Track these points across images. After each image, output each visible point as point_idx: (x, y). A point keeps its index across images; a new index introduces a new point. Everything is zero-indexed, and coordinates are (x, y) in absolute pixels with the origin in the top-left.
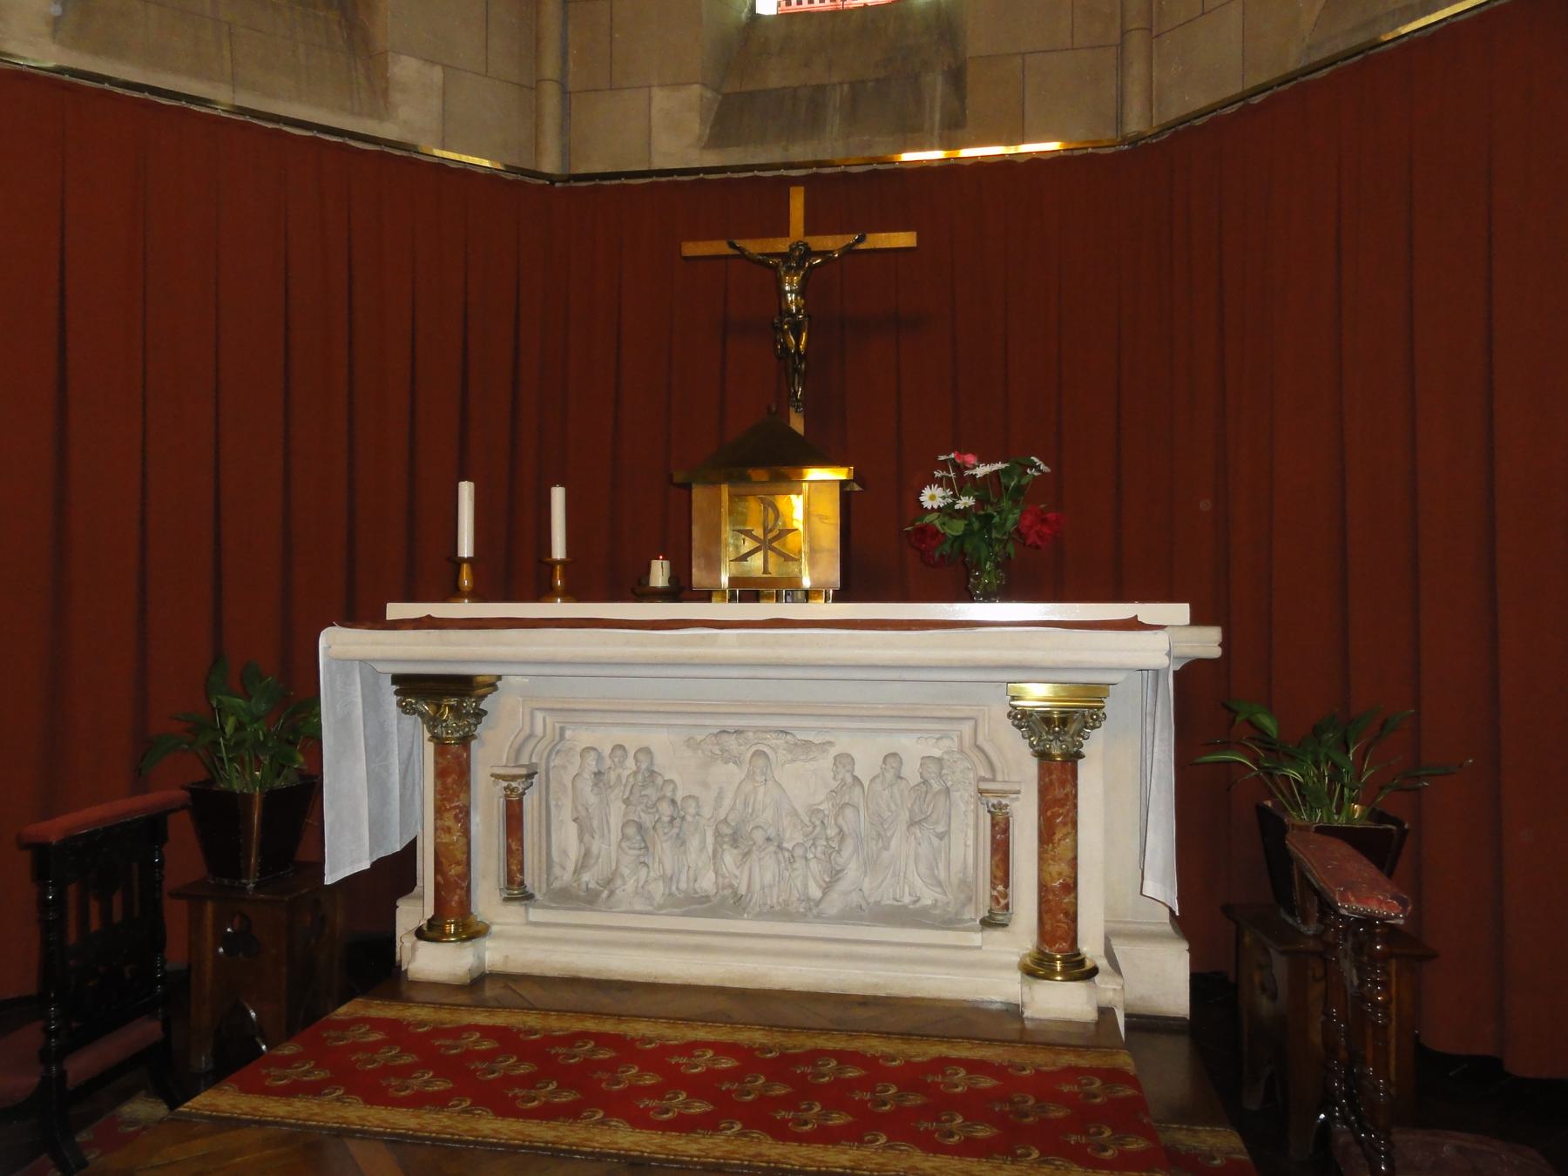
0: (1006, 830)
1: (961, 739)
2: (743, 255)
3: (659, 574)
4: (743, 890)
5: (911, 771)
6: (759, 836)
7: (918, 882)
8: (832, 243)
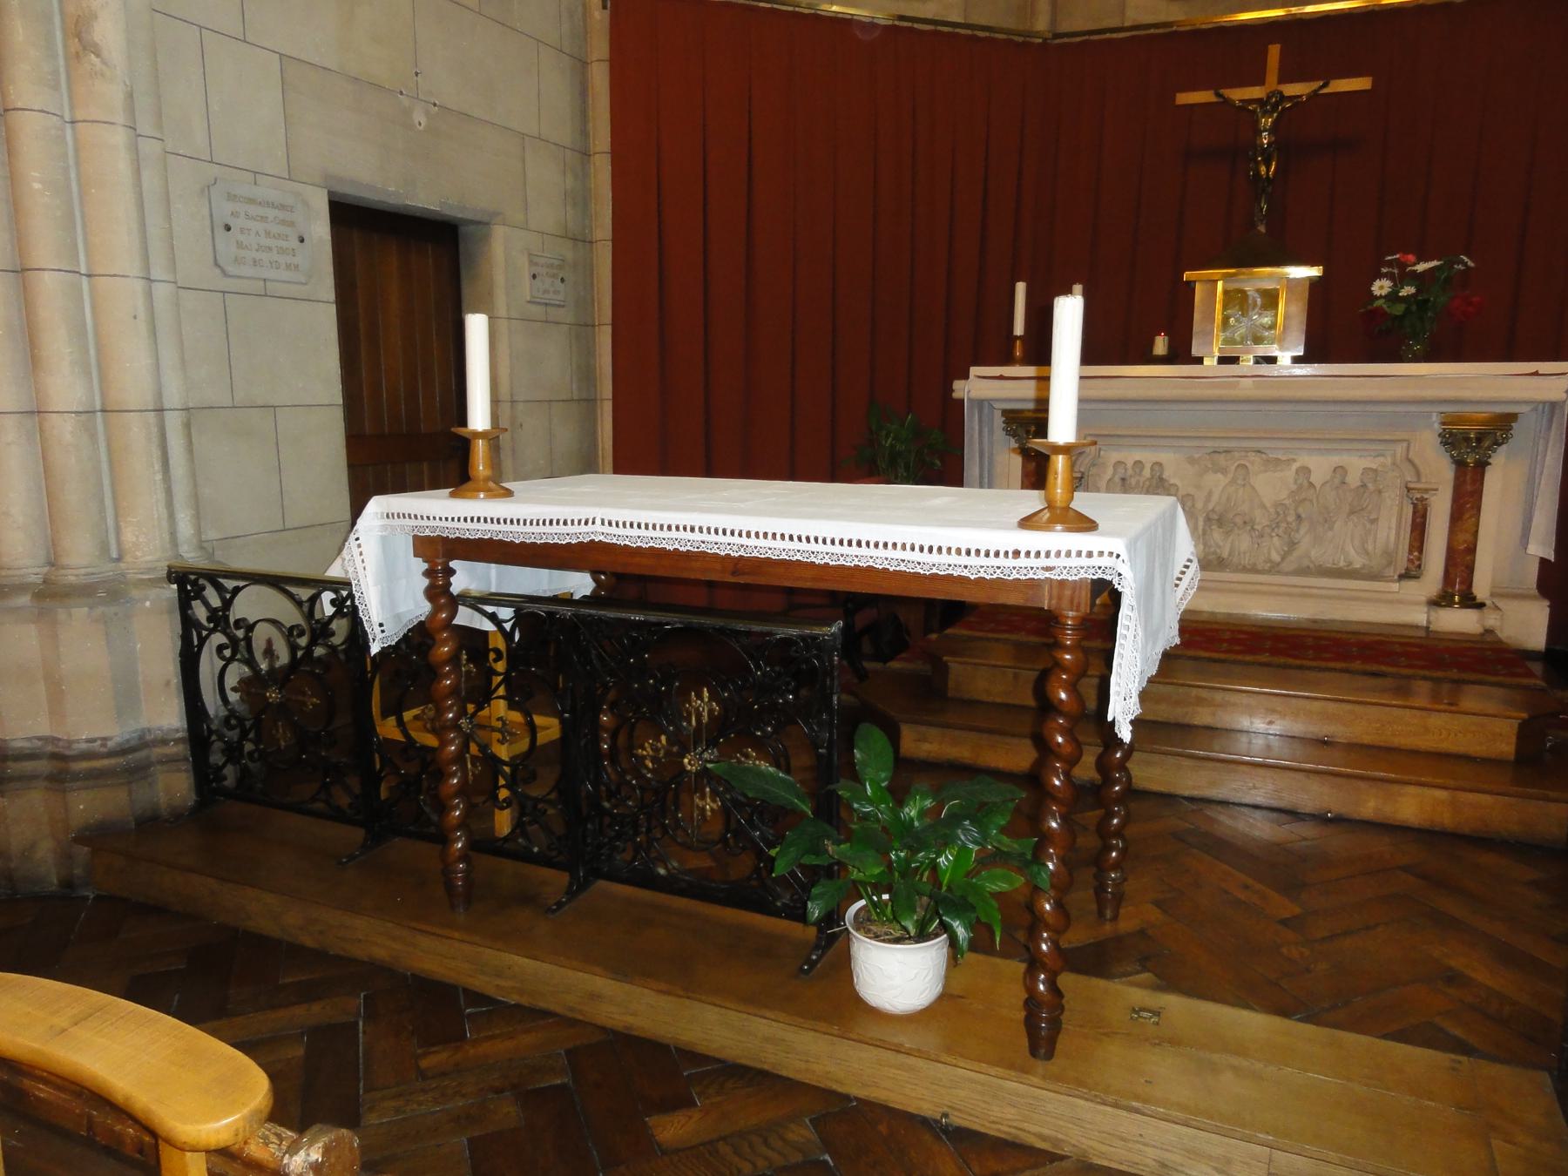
0: (1424, 516)
1: (1394, 456)
2: (1227, 102)
3: (1160, 346)
4: (1225, 555)
5: (1354, 479)
6: (1239, 520)
7: (1352, 552)
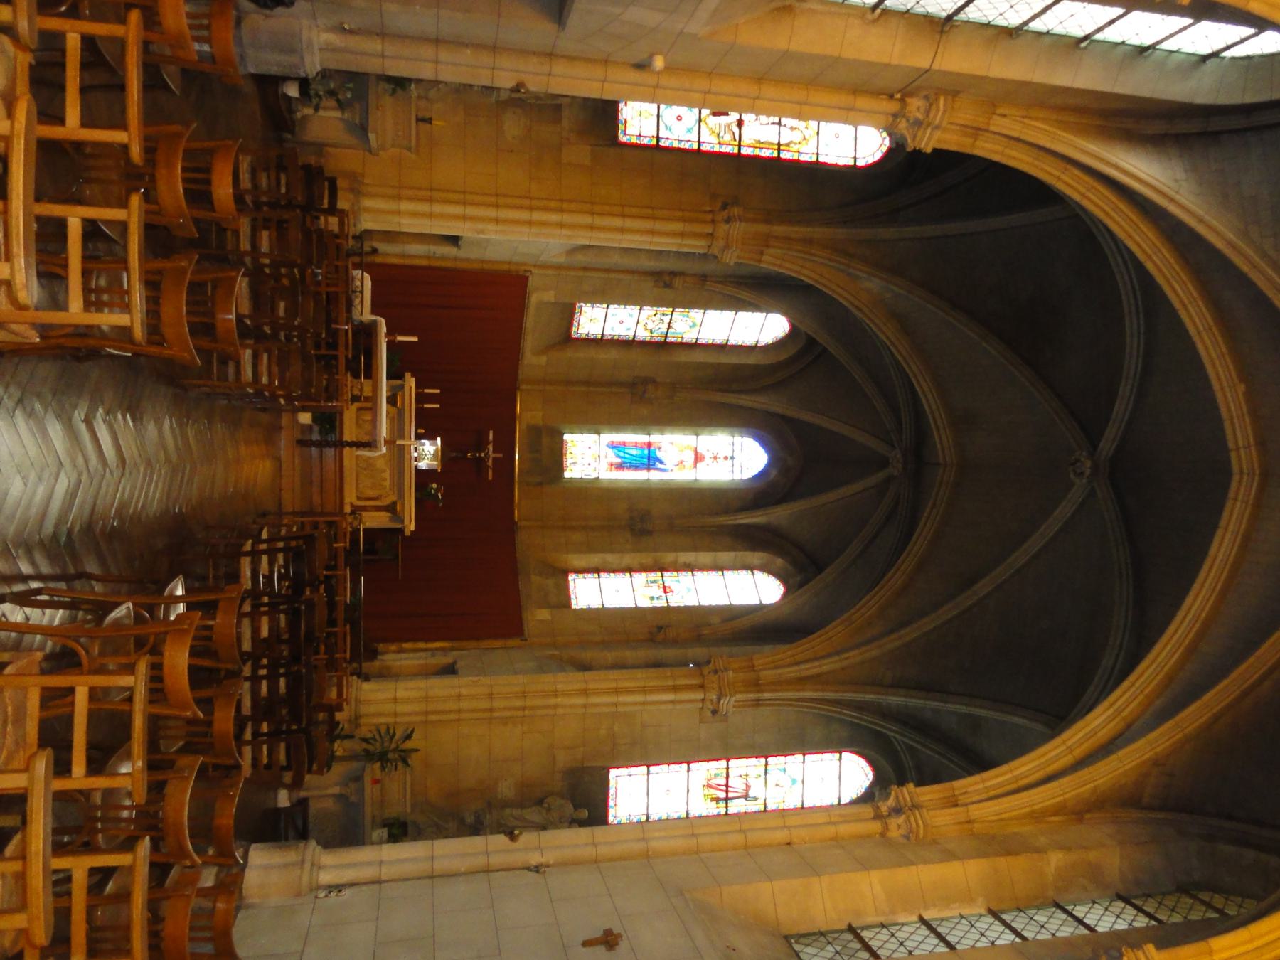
3: (420, 431)
8: (490, 463)
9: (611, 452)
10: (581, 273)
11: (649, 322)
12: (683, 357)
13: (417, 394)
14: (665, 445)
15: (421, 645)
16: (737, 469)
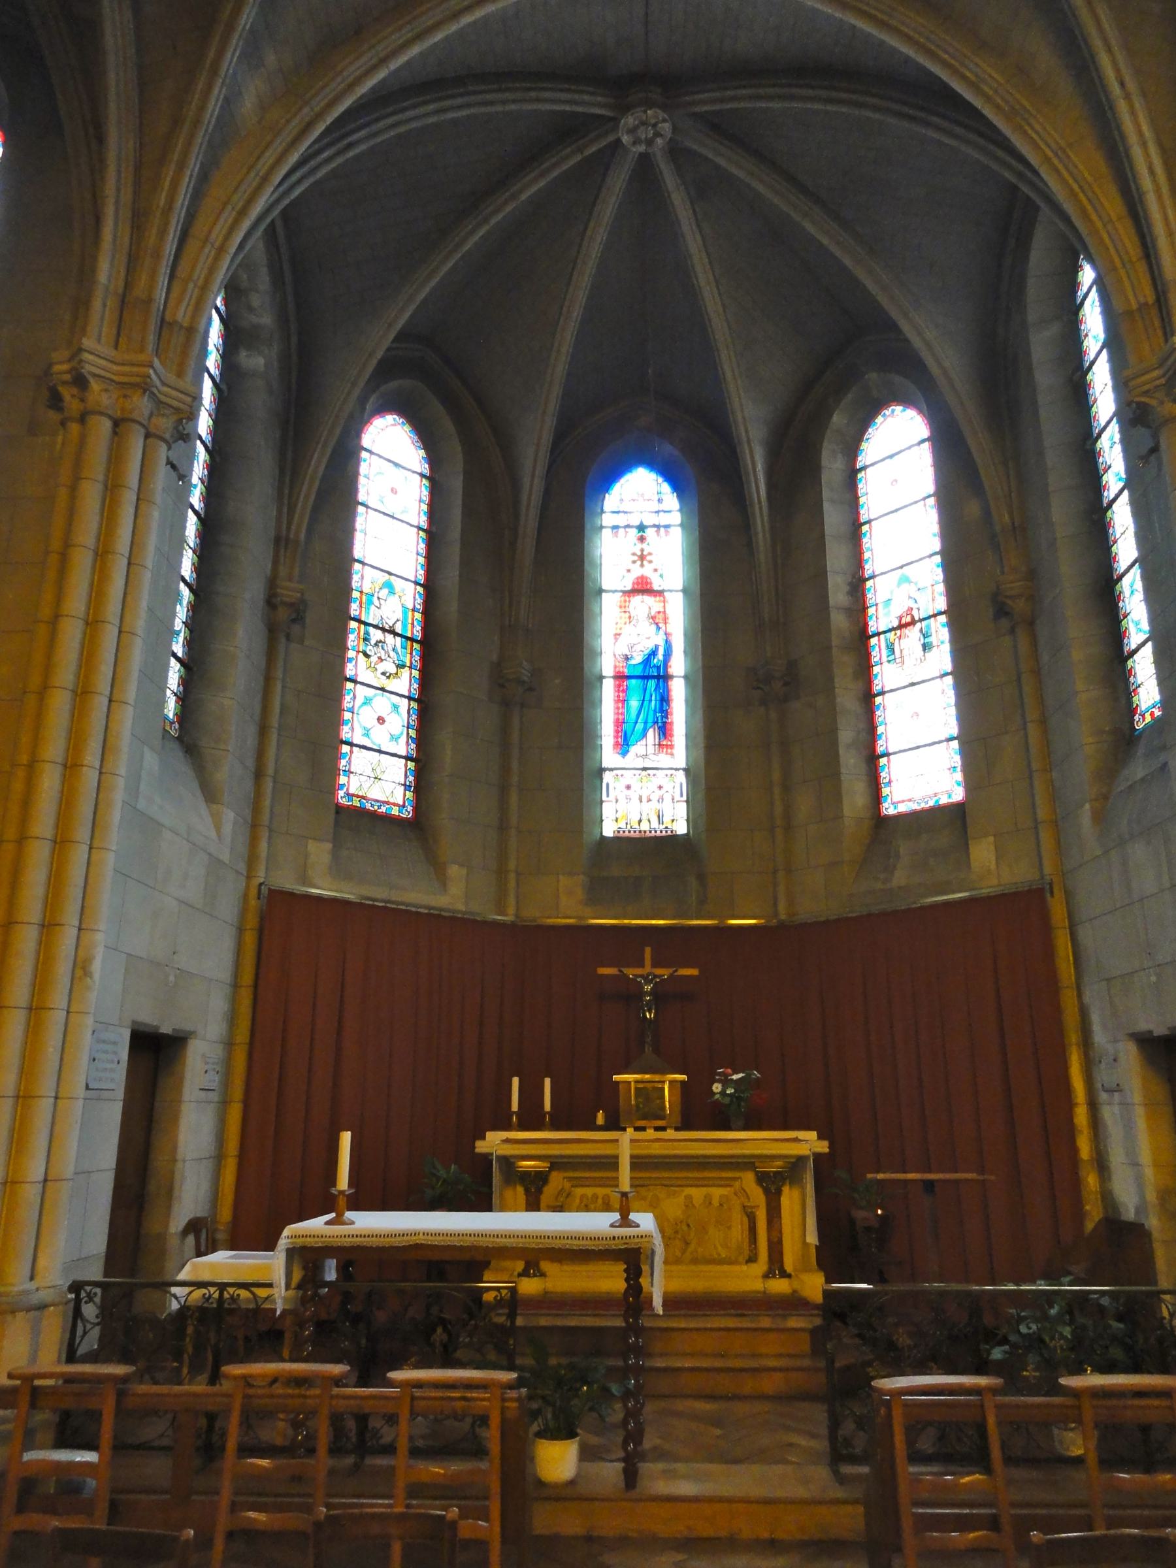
3: (600, 1118)
5: (716, 1203)
8: (665, 973)
9: (637, 749)
10: (268, 785)
11: (381, 667)
12: (451, 608)
13: (523, 1127)
14: (622, 649)
15: (1081, 1115)
16: (663, 519)
